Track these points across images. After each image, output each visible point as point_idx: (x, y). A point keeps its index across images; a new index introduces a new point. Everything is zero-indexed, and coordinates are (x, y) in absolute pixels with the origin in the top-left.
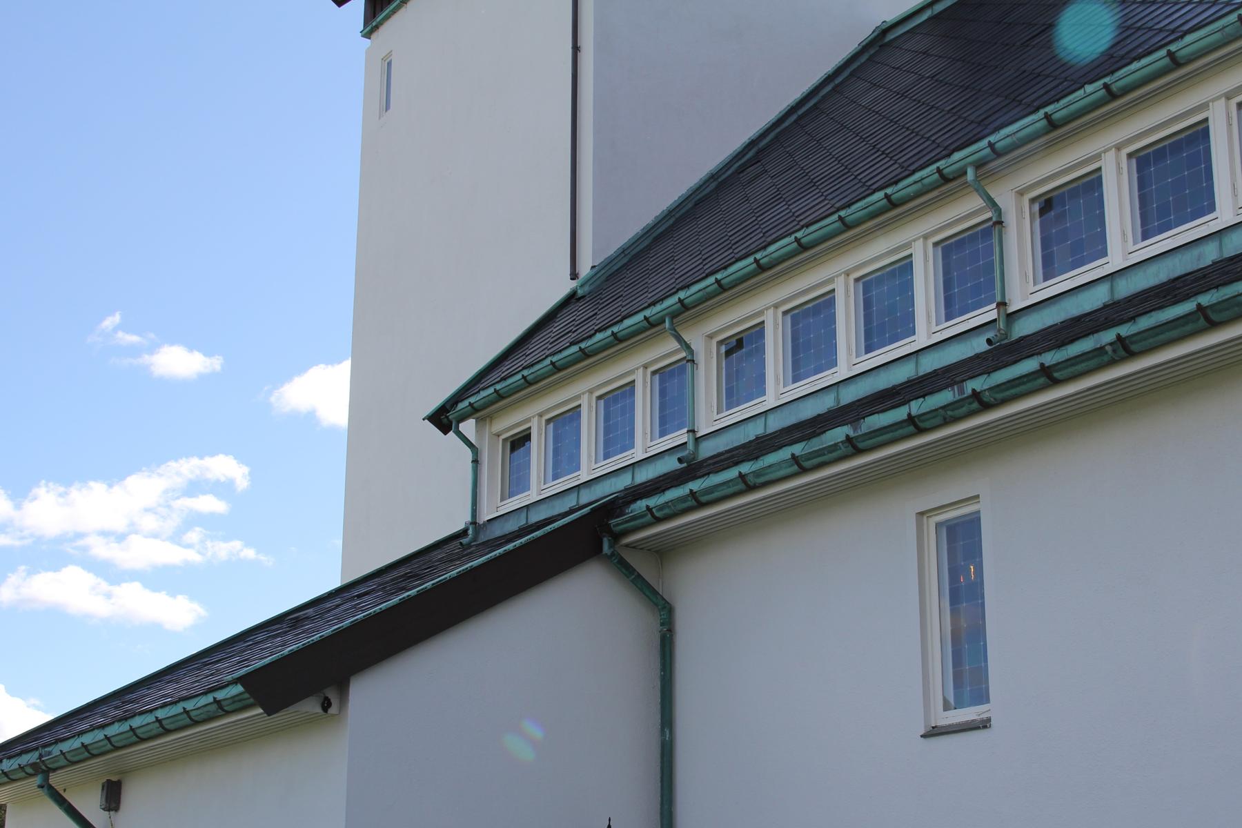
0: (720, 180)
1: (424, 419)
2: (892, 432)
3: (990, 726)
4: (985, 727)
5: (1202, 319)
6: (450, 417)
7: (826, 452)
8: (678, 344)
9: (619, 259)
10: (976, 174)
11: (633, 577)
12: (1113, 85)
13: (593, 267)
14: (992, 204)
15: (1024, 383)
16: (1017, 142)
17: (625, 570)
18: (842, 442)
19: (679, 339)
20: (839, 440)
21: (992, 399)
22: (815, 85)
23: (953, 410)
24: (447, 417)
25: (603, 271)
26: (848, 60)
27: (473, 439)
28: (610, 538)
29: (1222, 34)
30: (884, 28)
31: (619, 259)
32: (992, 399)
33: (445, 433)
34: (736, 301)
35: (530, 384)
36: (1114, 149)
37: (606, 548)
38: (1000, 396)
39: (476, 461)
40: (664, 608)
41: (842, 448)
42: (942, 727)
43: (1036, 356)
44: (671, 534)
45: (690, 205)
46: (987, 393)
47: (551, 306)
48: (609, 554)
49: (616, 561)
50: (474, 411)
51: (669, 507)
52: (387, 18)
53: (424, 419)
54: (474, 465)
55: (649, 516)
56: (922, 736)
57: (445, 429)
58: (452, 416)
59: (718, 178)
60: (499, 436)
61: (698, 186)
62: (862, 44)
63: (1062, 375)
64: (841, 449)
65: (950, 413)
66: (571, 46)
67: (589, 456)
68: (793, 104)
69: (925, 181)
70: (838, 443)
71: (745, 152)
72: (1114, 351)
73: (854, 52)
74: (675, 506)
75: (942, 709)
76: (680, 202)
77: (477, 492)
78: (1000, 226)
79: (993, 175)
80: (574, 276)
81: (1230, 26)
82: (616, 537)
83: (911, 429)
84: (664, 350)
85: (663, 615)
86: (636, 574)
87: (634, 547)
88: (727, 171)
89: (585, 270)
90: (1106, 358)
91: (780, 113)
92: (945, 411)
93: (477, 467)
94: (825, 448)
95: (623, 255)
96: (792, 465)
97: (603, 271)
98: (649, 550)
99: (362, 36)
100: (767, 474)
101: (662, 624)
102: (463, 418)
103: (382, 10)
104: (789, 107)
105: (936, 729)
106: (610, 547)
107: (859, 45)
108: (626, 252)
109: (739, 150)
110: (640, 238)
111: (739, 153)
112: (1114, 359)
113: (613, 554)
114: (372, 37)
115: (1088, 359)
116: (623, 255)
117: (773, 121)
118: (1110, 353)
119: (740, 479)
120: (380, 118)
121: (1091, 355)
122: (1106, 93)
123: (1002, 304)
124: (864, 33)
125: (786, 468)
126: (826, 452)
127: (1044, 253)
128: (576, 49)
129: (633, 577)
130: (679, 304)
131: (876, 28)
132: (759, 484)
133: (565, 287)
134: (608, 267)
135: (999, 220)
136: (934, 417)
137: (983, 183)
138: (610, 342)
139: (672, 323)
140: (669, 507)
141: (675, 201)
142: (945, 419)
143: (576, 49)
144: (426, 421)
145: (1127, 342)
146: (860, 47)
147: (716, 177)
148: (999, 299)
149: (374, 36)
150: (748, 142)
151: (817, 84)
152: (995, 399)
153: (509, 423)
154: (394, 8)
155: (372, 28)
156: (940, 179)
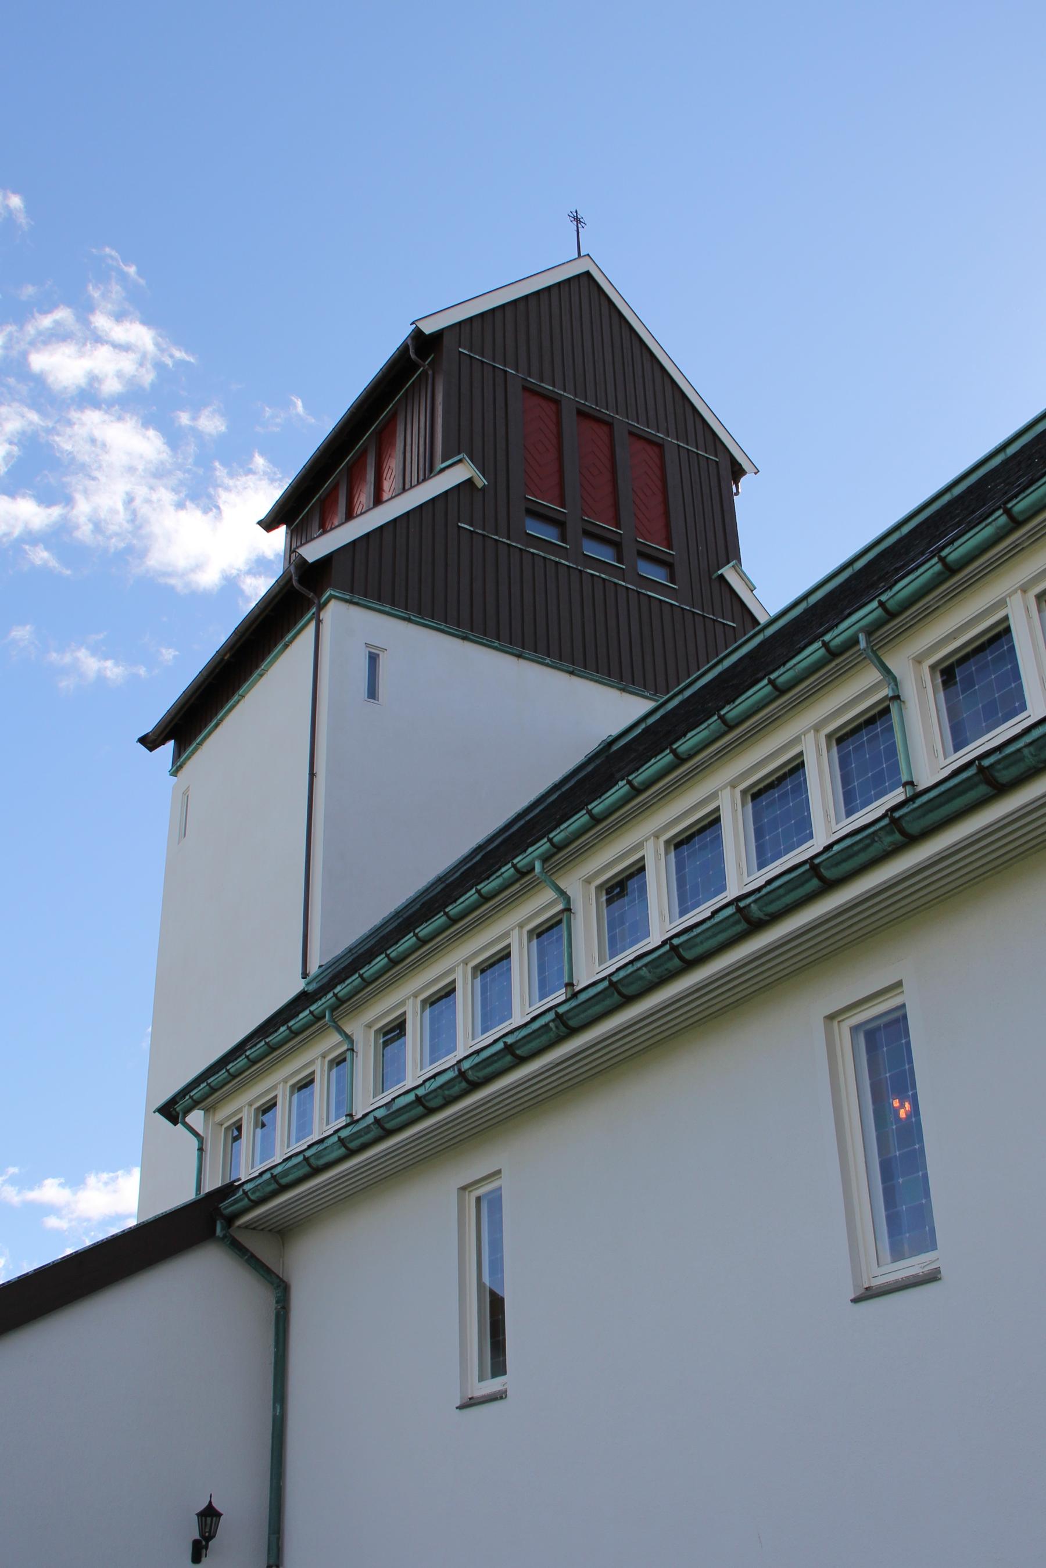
0: (447, 882)
1: (154, 1112)
2: (407, 1112)
3: (506, 1396)
4: (501, 1398)
5: (616, 994)
6: (177, 1109)
7: (363, 1134)
8: (340, 1037)
9: (346, 957)
10: (543, 866)
11: (246, 1257)
12: (634, 780)
13: (320, 966)
14: (562, 893)
15: (496, 1062)
16: (570, 836)
17: (238, 1249)
18: (372, 1123)
19: (340, 1030)
20: (370, 1122)
21: (476, 1079)
22: (541, 794)
23: (448, 1089)
24: (175, 1109)
25: (330, 970)
26: (574, 770)
27: (200, 1131)
28: (223, 1221)
29: (709, 731)
30: (608, 741)
31: (346, 957)
32: (476, 1079)
33: (175, 1123)
34: (387, 990)
35: (234, 1077)
36: (652, 838)
37: (219, 1231)
38: (481, 1074)
39: (201, 1149)
40: (279, 1286)
41: (374, 1129)
42: (477, 1398)
43: (510, 1035)
44: (277, 1216)
45: (418, 906)
46: (470, 1072)
47: (282, 1005)
48: (221, 1236)
49: (228, 1243)
50: (196, 1104)
51: (259, 1190)
52: (188, 758)
53: (154, 1112)
54: (200, 1153)
55: (246, 1200)
56: (457, 1408)
57: (174, 1120)
58: (179, 1108)
59: (446, 880)
60: (222, 1125)
61: (425, 888)
62: (589, 756)
63: (522, 1052)
64: (372, 1130)
65: (447, 1092)
66: (308, 772)
67: (282, 1141)
68: (521, 811)
69: (505, 875)
70: (370, 1124)
71: (472, 856)
72: (557, 1027)
73: (580, 763)
74: (263, 1189)
75: (477, 1381)
76: (407, 903)
77: (201, 1179)
78: (568, 913)
79: (563, 866)
80: (305, 975)
81: (713, 724)
82: (230, 1220)
83: (420, 1110)
84: (330, 1043)
85: (278, 1293)
86: (249, 1254)
87: (254, 1229)
88: (454, 874)
89: (313, 969)
90: (552, 1035)
91: (507, 820)
92: (443, 1091)
93: (202, 1154)
94: (361, 1130)
95: (350, 954)
96: (340, 1148)
97: (330, 970)
98: (270, 1230)
99: (170, 775)
100: (325, 1155)
101: (277, 1302)
102: (187, 1111)
103: (185, 750)
104: (516, 815)
105: (471, 1400)
106: (222, 1229)
107: (585, 757)
108: (354, 952)
109: (466, 855)
110: (368, 937)
111: (467, 857)
112: (559, 1035)
113: (225, 1237)
114: (178, 775)
115: (539, 1036)
116: (350, 954)
117: (501, 828)
118: (554, 1029)
119: (305, 1162)
120: (178, 844)
121: (539, 1032)
122: (630, 788)
123: (570, 985)
124: (591, 744)
125: (337, 1150)
126: (363, 1134)
127: (611, 934)
128: (312, 775)
129: (246, 1257)
130: (334, 998)
131: (602, 741)
132: (323, 1165)
133: (298, 985)
134: (333, 967)
135: (568, 907)
136: (436, 1097)
137: (553, 878)
138: (287, 1036)
139: (332, 1015)
140: (259, 1190)
141: (403, 903)
142: (445, 1098)
143: (312, 775)
144: (157, 1113)
145: (565, 1018)
146: (586, 759)
147: (443, 880)
148: (566, 980)
149: (180, 774)
150: (475, 846)
151: (544, 793)
152: (478, 1077)
153: (225, 1112)
154: (192, 750)
155: (177, 768)
156: (516, 873)
